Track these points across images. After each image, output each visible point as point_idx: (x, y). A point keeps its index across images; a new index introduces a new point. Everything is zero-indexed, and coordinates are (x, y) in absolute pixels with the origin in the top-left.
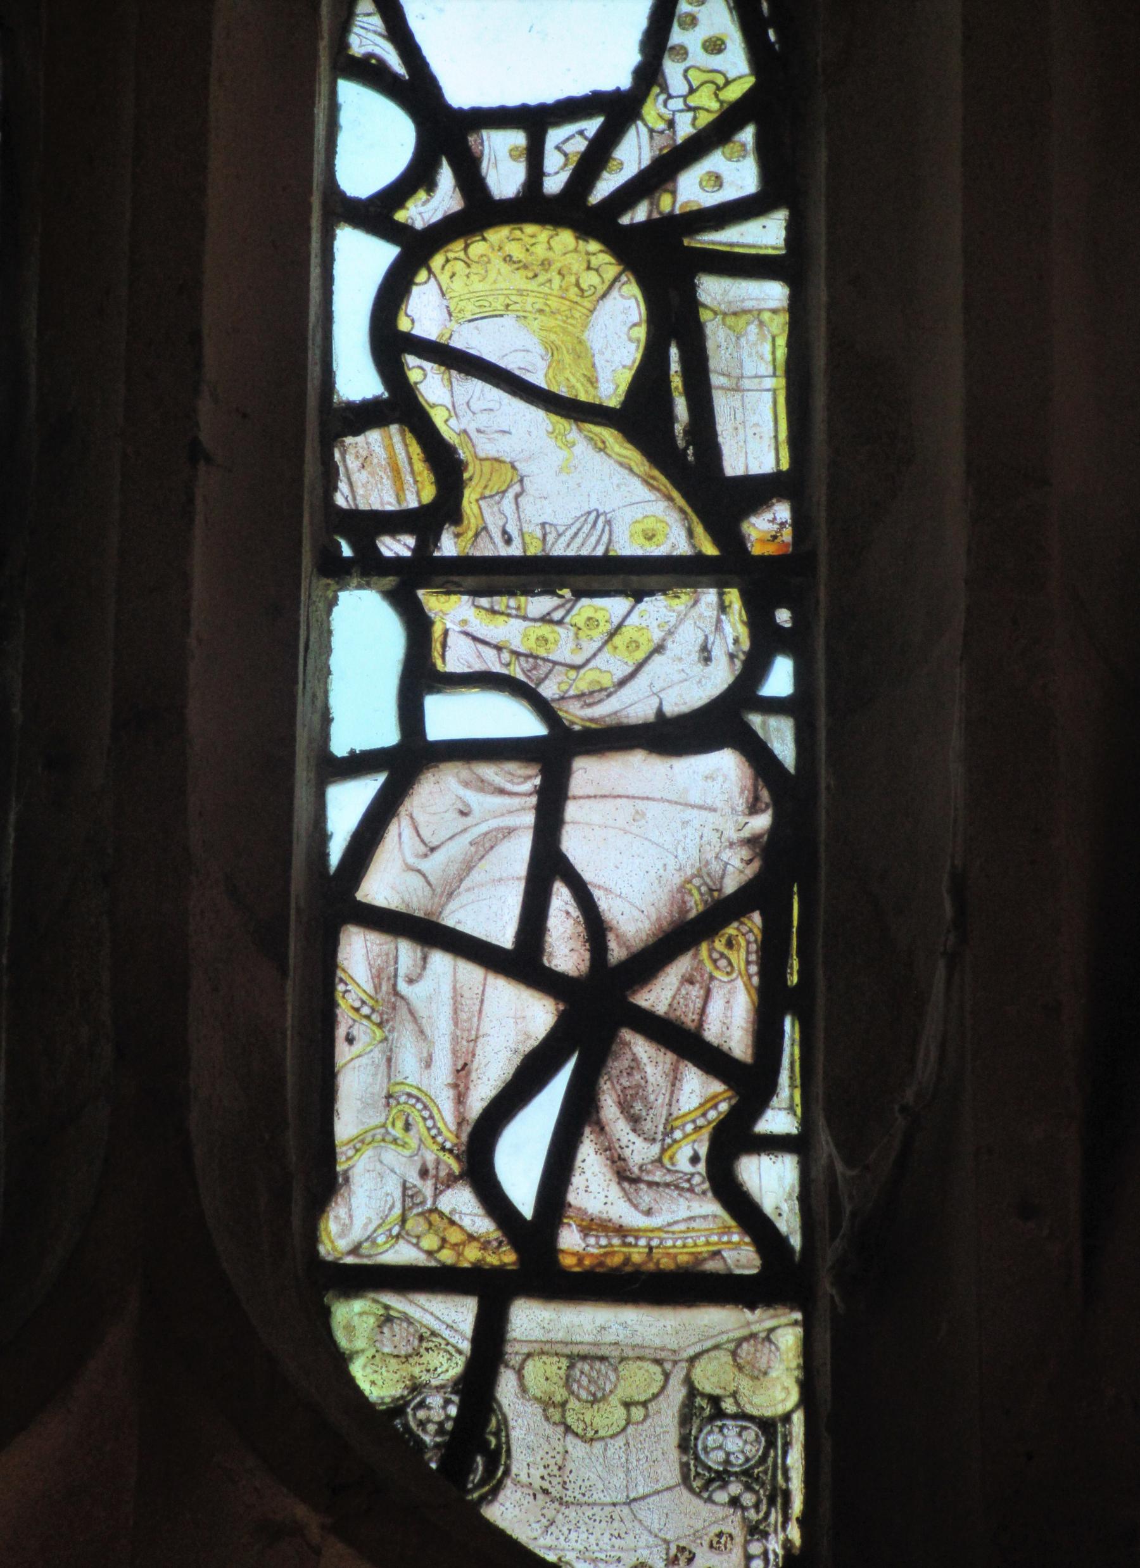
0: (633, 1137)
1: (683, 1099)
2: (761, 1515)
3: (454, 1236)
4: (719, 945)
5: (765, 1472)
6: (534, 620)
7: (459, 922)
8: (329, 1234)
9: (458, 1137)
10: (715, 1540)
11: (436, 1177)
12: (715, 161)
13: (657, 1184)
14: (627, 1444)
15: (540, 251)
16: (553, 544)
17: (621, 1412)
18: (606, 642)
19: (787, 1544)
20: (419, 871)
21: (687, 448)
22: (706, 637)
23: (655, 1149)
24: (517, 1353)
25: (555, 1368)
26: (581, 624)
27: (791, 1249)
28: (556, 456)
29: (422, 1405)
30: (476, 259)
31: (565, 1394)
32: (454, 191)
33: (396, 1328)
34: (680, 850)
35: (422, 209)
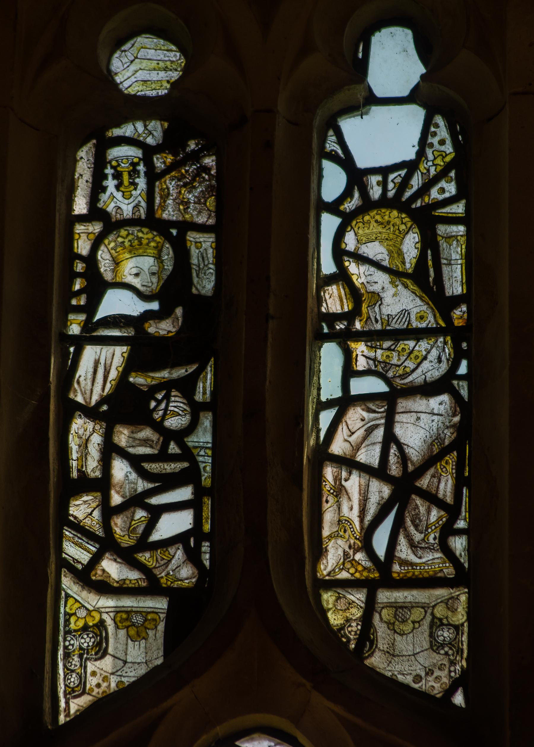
0: (415, 532)
1: (431, 518)
2: (454, 657)
3: (360, 568)
4: (443, 463)
5: (456, 643)
6: (385, 349)
7: (361, 459)
8: (321, 569)
9: (361, 534)
10: (440, 666)
11: (354, 548)
12: (443, 184)
13: (423, 548)
14: (413, 636)
15: (386, 218)
16: (391, 322)
17: (411, 625)
18: (408, 357)
19: (462, 667)
20: (348, 441)
21: (433, 286)
22: (440, 353)
23: (423, 535)
24: (379, 607)
25: (392, 611)
26: (400, 350)
27: (465, 567)
28: (391, 290)
29: (350, 626)
30: (366, 222)
31: (394, 619)
32: (359, 198)
33: (342, 600)
34: (431, 430)
35: (349, 205)
